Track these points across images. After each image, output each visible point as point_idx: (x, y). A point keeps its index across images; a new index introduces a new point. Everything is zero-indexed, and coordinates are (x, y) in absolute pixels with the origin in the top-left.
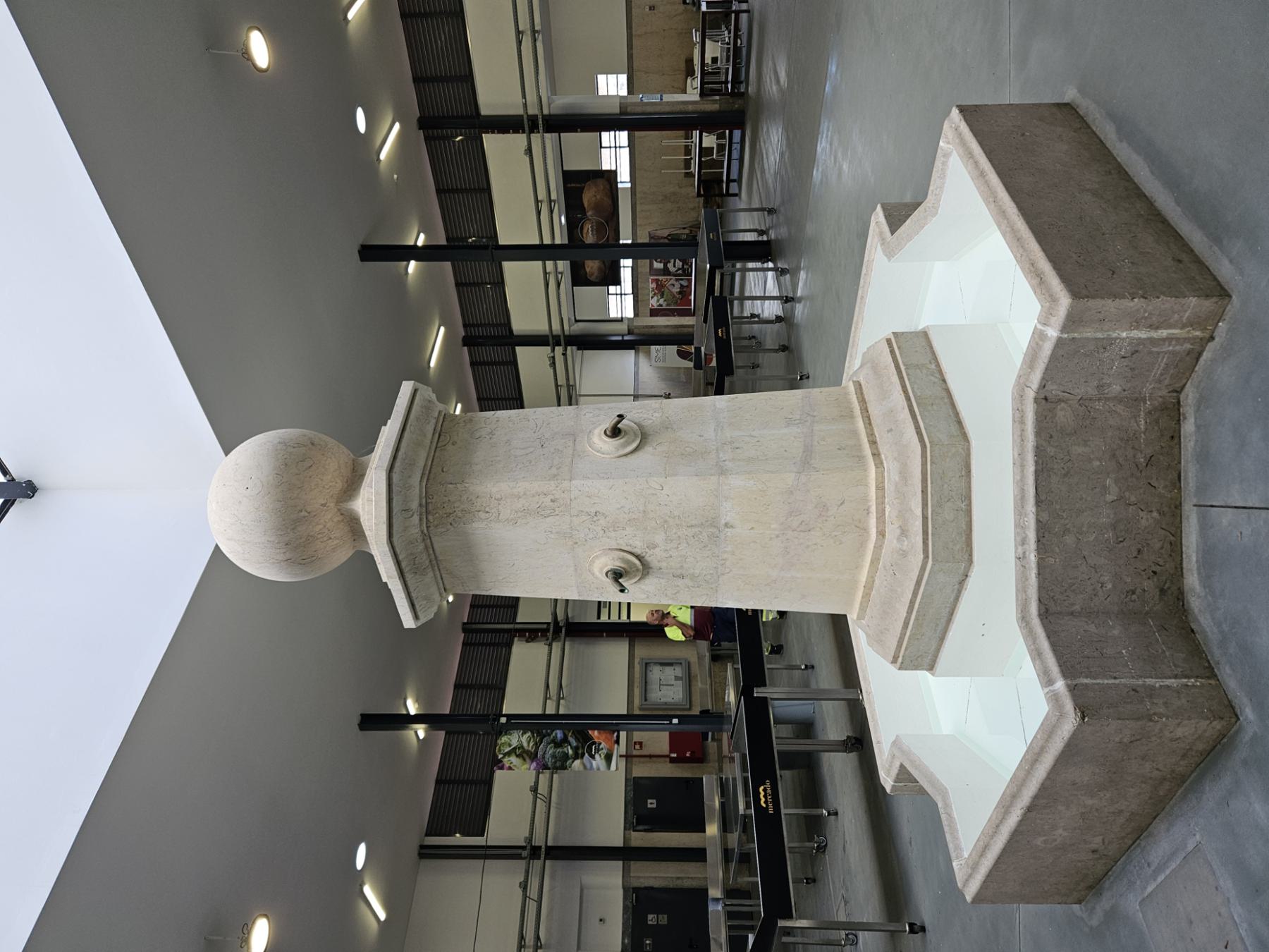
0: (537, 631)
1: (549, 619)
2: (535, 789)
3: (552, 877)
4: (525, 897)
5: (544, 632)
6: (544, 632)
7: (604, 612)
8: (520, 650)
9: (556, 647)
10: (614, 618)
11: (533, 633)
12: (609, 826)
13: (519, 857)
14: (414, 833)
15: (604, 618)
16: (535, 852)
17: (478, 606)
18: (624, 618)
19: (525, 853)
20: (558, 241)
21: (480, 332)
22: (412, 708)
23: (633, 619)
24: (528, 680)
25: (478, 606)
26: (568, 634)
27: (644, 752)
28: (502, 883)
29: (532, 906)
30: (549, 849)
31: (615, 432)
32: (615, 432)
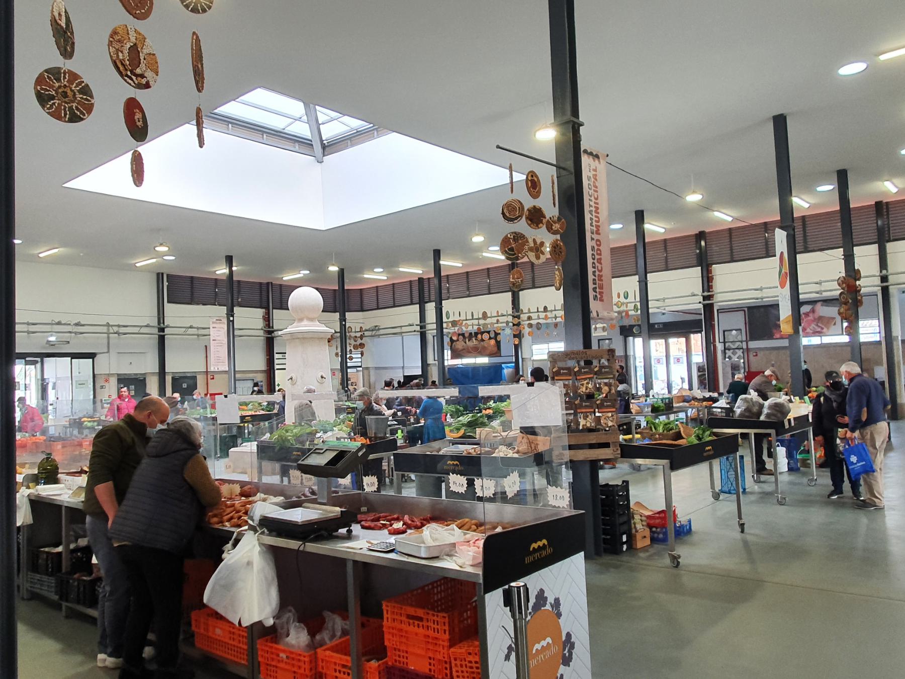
0: (269, 321)
1: (275, 328)
2: (191, 327)
3: (150, 338)
4: (141, 327)
5: (268, 326)
6: (268, 326)
7: (280, 356)
8: (260, 312)
9: (261, 333)
10: (276, 362)
11: (268, 319)
12: (174, 366)
13: (159, 323)
14: (166, 271)
15: (276, 356)
16: (162, 330)
17: (192, 283)
18: (277, 367)
19: (162, 325)
20: (801, 297)
21: (426, 286)
22: (234, 269)
23: (276, 372)
24: (249, 318)
25: (192, 283)
26: (267, 338)
27: (210, 381)
28: (148, 315)
29: (136, 330)
30: (887, 287)
31: (322, 377)
32: (322, 377)
